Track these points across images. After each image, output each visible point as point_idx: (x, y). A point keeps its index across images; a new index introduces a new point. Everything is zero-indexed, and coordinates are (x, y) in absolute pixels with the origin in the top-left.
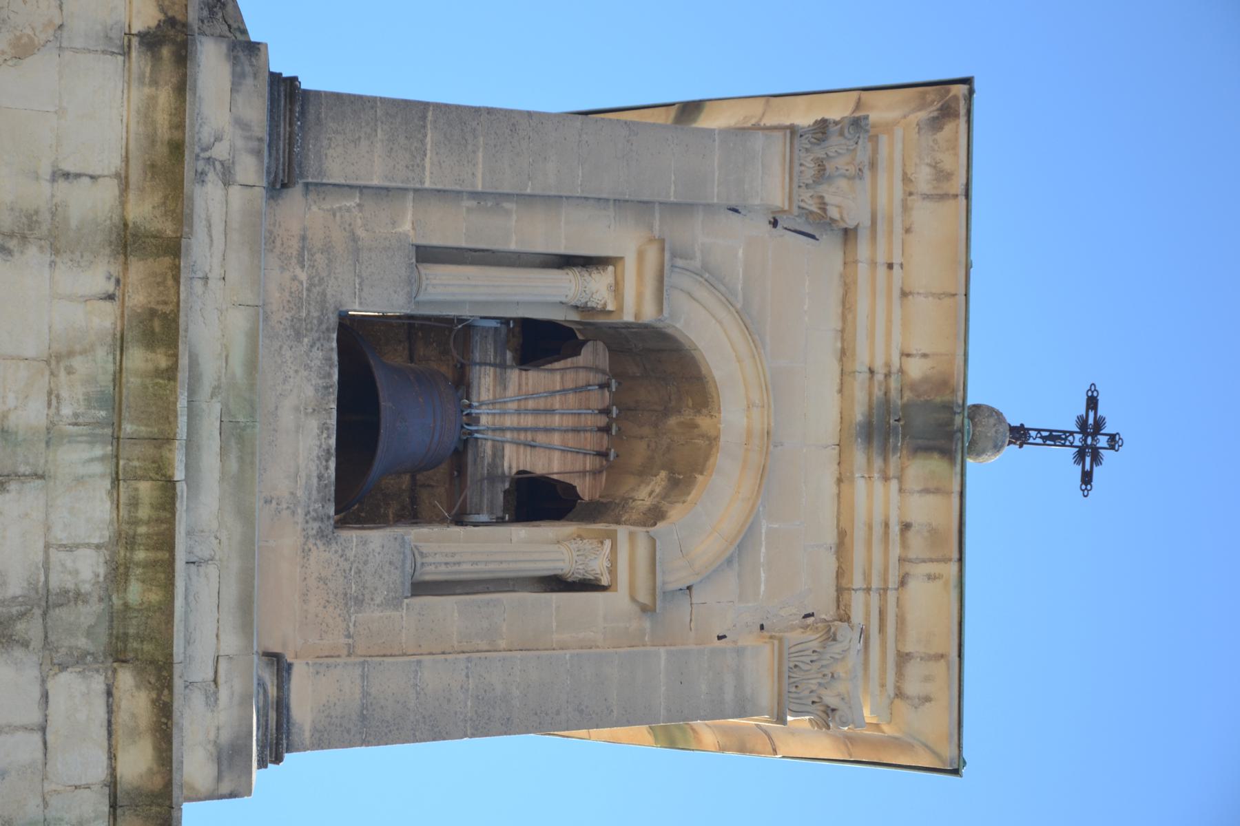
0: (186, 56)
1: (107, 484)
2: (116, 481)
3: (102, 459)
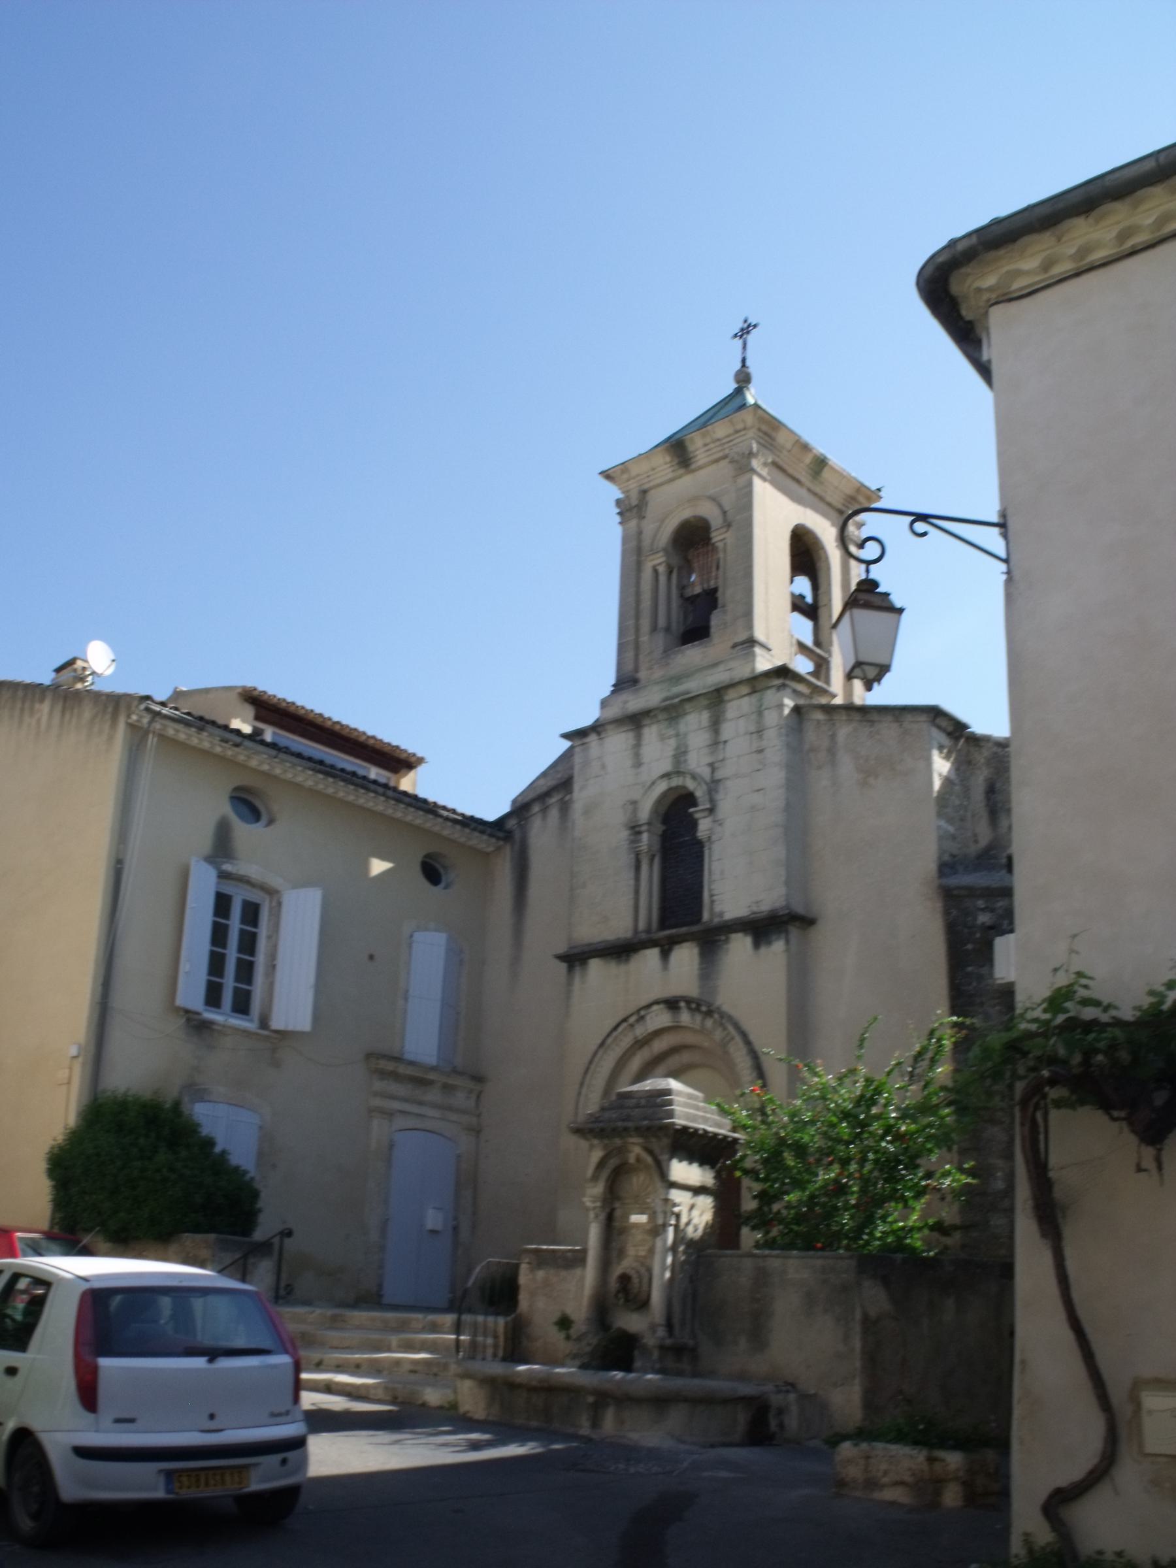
0: (814, 1248)
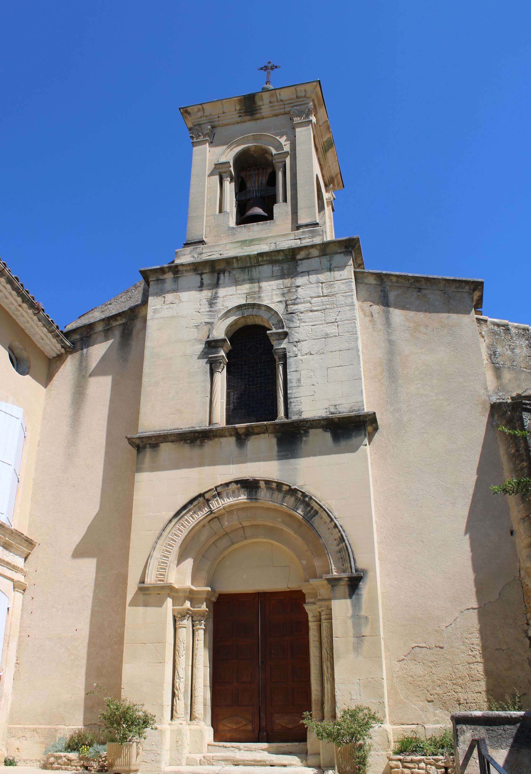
1: (260, 267)
2: (260, 265)
3: (255, 269)
